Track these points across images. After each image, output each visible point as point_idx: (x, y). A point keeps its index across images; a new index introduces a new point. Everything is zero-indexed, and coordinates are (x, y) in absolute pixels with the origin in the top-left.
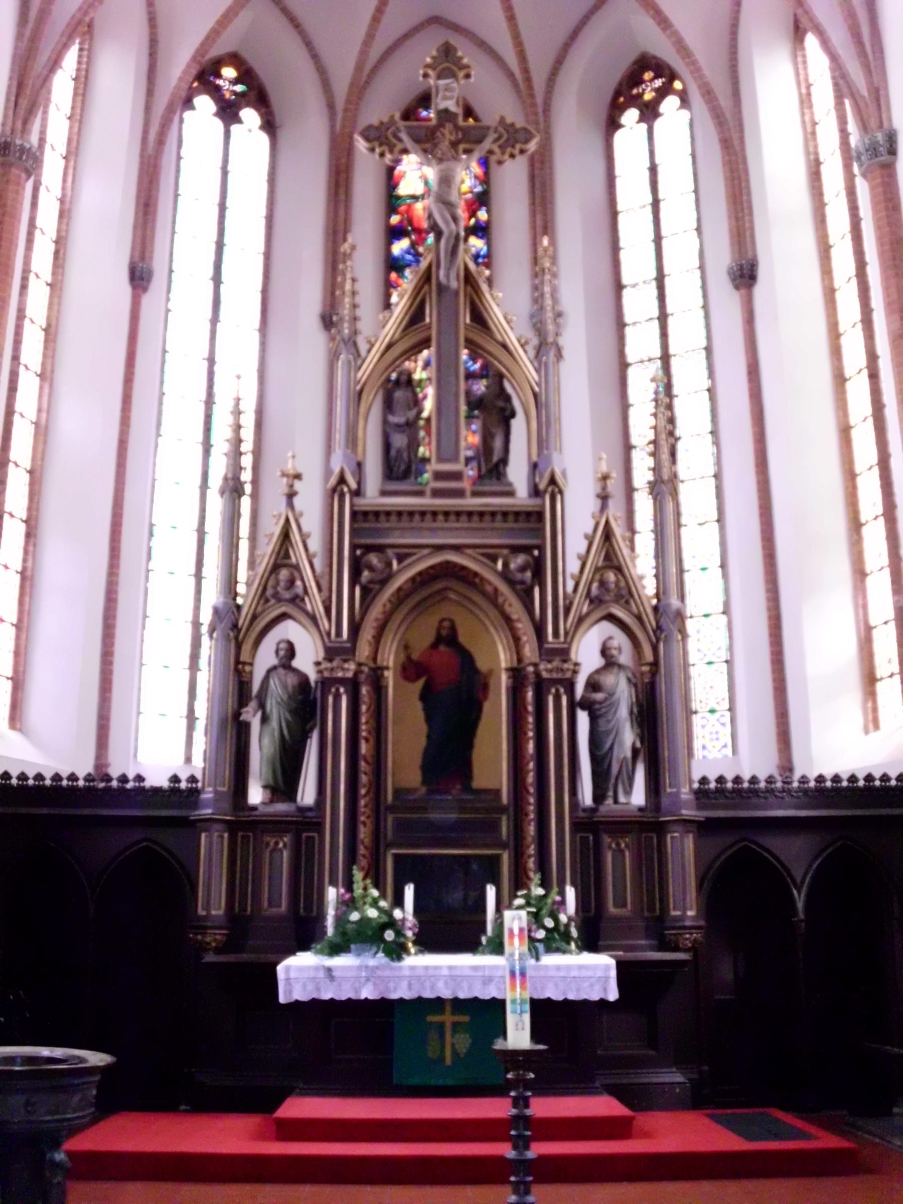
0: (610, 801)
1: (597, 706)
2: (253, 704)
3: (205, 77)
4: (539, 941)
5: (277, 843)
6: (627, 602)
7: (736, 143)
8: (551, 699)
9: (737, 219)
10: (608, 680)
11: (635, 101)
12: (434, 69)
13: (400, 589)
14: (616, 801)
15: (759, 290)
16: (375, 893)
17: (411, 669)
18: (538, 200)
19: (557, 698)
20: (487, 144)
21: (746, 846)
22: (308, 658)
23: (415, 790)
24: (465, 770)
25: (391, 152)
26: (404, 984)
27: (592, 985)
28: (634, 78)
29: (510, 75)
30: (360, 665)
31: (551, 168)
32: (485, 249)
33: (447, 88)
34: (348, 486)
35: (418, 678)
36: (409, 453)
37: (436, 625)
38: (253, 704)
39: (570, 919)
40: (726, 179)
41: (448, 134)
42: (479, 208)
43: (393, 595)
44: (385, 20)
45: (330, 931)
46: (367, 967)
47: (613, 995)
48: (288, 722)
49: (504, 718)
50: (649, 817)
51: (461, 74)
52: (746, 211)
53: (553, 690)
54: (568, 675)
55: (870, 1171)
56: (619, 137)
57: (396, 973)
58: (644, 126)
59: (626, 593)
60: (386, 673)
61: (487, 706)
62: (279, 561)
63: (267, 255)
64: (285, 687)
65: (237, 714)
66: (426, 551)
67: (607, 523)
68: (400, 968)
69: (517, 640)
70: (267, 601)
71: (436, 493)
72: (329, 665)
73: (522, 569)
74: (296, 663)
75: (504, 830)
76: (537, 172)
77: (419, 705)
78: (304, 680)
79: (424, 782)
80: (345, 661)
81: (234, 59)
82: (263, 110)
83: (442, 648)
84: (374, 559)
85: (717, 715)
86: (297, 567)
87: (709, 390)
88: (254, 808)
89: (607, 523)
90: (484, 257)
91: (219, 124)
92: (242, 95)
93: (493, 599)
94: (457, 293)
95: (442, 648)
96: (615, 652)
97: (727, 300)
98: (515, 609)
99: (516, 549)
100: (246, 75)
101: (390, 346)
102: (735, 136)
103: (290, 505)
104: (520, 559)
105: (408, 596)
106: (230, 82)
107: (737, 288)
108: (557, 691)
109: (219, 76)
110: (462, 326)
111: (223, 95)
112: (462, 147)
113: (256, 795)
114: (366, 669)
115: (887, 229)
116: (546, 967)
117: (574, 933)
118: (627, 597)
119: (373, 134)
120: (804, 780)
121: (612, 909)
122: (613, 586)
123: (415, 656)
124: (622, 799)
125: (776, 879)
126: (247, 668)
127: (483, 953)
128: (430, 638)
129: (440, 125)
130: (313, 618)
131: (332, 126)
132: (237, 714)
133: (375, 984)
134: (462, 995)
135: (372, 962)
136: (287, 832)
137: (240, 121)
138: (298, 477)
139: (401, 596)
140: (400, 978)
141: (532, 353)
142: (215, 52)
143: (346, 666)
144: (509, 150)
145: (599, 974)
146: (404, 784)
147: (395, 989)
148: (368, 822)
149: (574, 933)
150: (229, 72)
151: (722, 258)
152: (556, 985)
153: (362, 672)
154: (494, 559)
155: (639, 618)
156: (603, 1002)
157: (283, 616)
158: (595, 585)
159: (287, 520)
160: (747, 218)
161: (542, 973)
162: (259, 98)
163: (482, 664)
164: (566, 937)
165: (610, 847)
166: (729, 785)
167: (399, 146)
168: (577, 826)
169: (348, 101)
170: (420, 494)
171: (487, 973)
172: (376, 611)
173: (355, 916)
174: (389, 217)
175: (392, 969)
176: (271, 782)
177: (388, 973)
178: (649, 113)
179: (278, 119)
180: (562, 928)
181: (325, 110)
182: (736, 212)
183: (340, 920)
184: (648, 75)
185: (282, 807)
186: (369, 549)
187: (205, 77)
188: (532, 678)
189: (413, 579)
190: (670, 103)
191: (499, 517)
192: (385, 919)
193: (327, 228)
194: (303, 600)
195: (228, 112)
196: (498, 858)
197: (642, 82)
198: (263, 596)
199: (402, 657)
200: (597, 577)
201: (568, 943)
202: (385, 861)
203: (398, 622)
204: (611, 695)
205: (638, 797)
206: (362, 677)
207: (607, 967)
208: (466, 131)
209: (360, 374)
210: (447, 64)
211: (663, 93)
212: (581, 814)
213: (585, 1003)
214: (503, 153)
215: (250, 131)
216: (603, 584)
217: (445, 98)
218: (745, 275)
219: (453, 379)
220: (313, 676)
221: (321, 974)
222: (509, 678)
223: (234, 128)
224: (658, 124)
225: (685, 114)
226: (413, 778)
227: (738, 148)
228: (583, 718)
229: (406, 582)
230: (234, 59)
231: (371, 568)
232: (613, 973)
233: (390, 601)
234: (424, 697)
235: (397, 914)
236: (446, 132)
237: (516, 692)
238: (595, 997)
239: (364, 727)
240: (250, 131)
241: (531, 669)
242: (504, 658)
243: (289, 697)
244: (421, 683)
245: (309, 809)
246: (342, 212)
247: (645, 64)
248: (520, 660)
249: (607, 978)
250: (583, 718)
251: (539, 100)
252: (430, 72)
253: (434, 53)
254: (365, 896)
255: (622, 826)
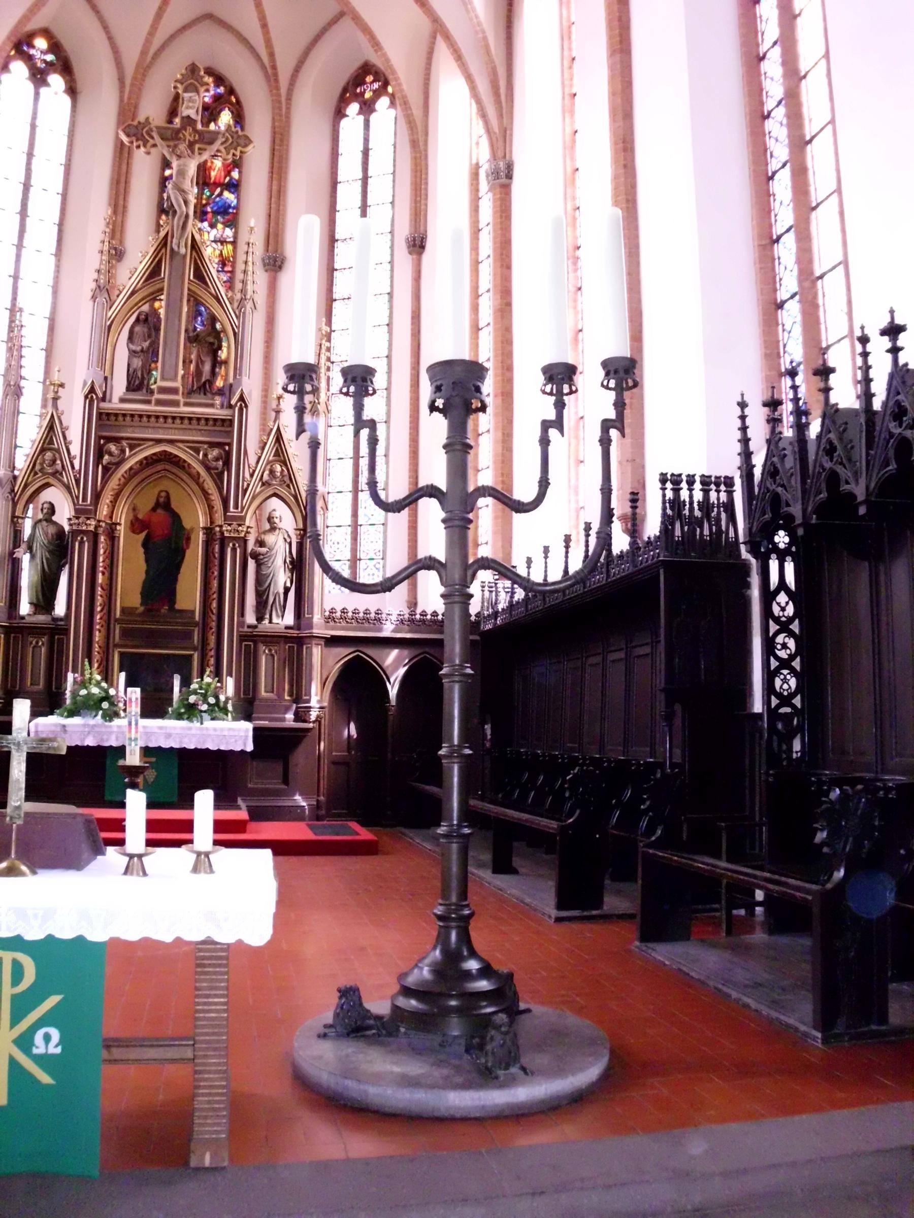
0: (266, 621)
1: (262, 557)
2: (24, 546)
3: (21, 46)
4: (205, 712)
5: (37, 643)
6: (288, 486)
7: (421, 144)
8: (229, 550)
9: (416, 202)
10: (270, 539)
11: (358, 97)
12: (182, 84)
13: (131, 469)
14: (270, 622)
15: (426, 257)
16: (99, 678)
17: (137, 525)
18: (275, 170)
19: (234, 550)
20: (217, 145)
21: (358, 655)
22: (64, 515)
23: (137, 608)
24: (171, 595)
25: (145, 146)
26: (113, 737)
27: (236, 741)
28: (358, 80)
29: (263, 67)
30: (99, 521)
31: (287, 146)
32: (235, 201)
33: (191, 100)
34: (96, 394)
35: (141, 532)
36: (142, 372)
37: (157, 493)
38: (24, 546)
39: (227, 699)
40: (412, 170)
41: (188, 134)
42: (232, 169)
43: (126, 472)
44: (166, 15)
45: (68, 702)
46: (88, 725)
47: (250, 747)
48: (47, 559)
49: (200, 561)
50: (294, 633)
51: (202, 89)
52: (423, 197)
53: (231, 545)
54: (242, 535)
55: (387, 854)
56: (344, 123)
57: (109, 730)
58: (362, 118)
59: (289, 479)
60: (118, 527)
61: (188, 553)
62: (45, 446)
63: (64, 196)
64: (46, 534)
65: (12, 553)
66: (151, 443)
67: (278, 429)
68: (110, 727)
69: (211, 507)
70: (36, 474)
71: (159, 402)
72: (76, 521)
73: (217, 459)
74: (54, 518)
75: (196, 638)
76: (277, 147)
77: (142, 550)
78: (61, 530)
79: (142, 604)
80: (88, 519)
81: (46, 33)
82: (67, 78)
83: (159, 511)
84: (113, 447)
85: (374, 562)
86: (58, 451)
87: (388, 325)
88: (23, 618)
89: (278, 429)
90: (234, 208)
91: (30, 86)
92: (50, 64)
93: (196, 478)
94: (184, 256)
95: (159, 511)
96: (276, 520)
97: (404, 260)
98: (210, 485)
99: (212, 445)
100: (55, 47)
101: (133, 294)
102: (421, 139)
103: (55, 406)
104: (215, 452)
105: (136, 474)
106: (42, 52)
107: (410, 253)
108: (234, 545)
109: (33, 47)
110: (186, 281)
111: (36, 63)
112: (197, 146)
113: (25, 608)
114: (103, 524)
115: (499, 232)
116: (207, 729)
117: (230, 707)
118: (288, 482)
119: (133, 131)
120: (424, 614)
121: (263, 693)
122: (279, 474)
123: (140, 516)
124: (275, 620)
125: (377, 679)
126: (20, 521)
127: (170, 718)
128: (151, 504)
129: (183, 127)
130: (68, 488)
131: (121, 100)
132: (12, 553)
133: (94, 737)
134: (151, 745)
135: (92, 722)
136: (45, 634)
137: (48, 85)
138: (62, 385)
139: (132, 473)
140: (111, 733)
141: (236, 304)
142: (31, 26)
143: (88, 522)
144: (232, 151)
145: (242, 734)
146: (129, 604)
147: (107, 740)
148: (102, 629)
149: (230, 707)
150: (41, 43)
151: (404, 230)
152: (213, 741)
153: (101, 526)
154: (197, 451)
155: (295, 497)
156: (243, 752)
157: (47, 485)
158: (267, 472)
159: (52, 416)
160: (423, 202)
161: (205, 732)
162: (65, 67)
163: (187, 524)
164: (225, 710)
165: (264, 651)
166: (361, 615)
167: (152, 142)
168: (243, 638)
169: (134, 78)
170: (148, 402)
171: (168, 731)
172: (114, 483)
173: (83, 692)
174: (164, 170)
175: (106, 727)
176: (35, 601)
177: (103, 729)
178: (367, 108)
179: (80, 86)
180: (222, 704)
181: (117, 82)
182: (416, 196)
183: (75, 694)
184: (369, 79)
185: (42, 618)
186: (109, 439)
187: (21, 46)
188: (218, 535)
189: (140, 462)
190: (383, 103)
191: (203, 422)
192: (103, 694)
193: (112, 179)
194: (61, 474)
195: (39, 77)
196: (191, 656)
197: (364, 83)
198: (32, 469)
199: (131, 517)
200: (268, 467)
201: (227, 715)
202: (113, 656)
203: (130, 490)
204: (271, 549)
205: (289, 619)
206: (100, 530)
207: (247, 730)
208: (200, 133)
209: (110, 314)
210: (192, 81)
211: (378, 94)
212: (246, 629)
213: (231, 752)
214: (228, 154)
215: (56, 93)
216: (272, 472)
217: (187, 108)
218: (418, 245)
219: (177, 322)
220: (67, 528)
221: (58, 729)
222: (204, 534)
223: (43, 90)
224: (373, 118)
225: (392, 112)
226: (135, 601)
227: (422, 148)
228: (251, 564)
229: (136, 463)
230: (46, 33)
231: (110, 454)
232: (251, 734)
233: (123, 476)
234: (145, 545)
235: (112, 692)
236: (187, 134)
237: (208, 544)
238: (238, 748)
239: (101, 564)
240: (56, 93)
241: (218, 529)
242: (202, 521)
243: (49, 542)
244: (144, 534)
245: (61, 620)
246: (124, 167)
247: (366, 69)
248: (212, 522)
249: (247, 737)
250: (251, 564)
251: (283, 91)
252: (179, 85)
253: (183, 71)
254: (90, 679)
255: (272, 639)
